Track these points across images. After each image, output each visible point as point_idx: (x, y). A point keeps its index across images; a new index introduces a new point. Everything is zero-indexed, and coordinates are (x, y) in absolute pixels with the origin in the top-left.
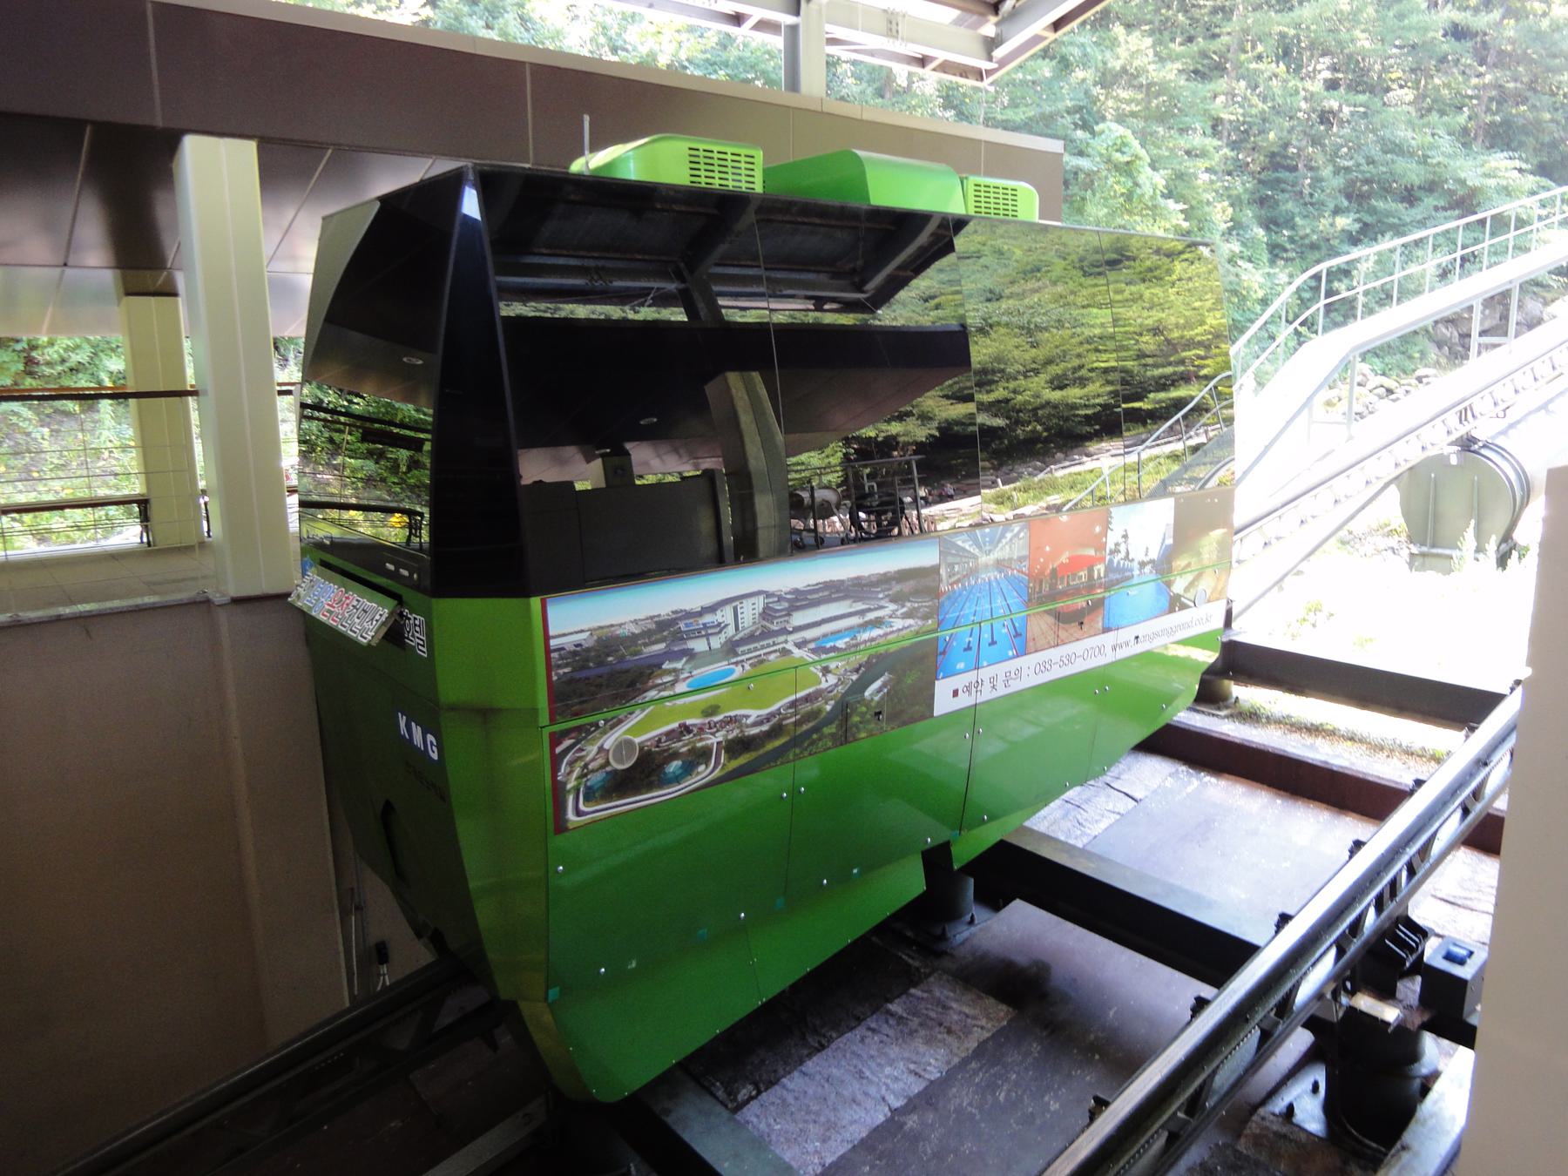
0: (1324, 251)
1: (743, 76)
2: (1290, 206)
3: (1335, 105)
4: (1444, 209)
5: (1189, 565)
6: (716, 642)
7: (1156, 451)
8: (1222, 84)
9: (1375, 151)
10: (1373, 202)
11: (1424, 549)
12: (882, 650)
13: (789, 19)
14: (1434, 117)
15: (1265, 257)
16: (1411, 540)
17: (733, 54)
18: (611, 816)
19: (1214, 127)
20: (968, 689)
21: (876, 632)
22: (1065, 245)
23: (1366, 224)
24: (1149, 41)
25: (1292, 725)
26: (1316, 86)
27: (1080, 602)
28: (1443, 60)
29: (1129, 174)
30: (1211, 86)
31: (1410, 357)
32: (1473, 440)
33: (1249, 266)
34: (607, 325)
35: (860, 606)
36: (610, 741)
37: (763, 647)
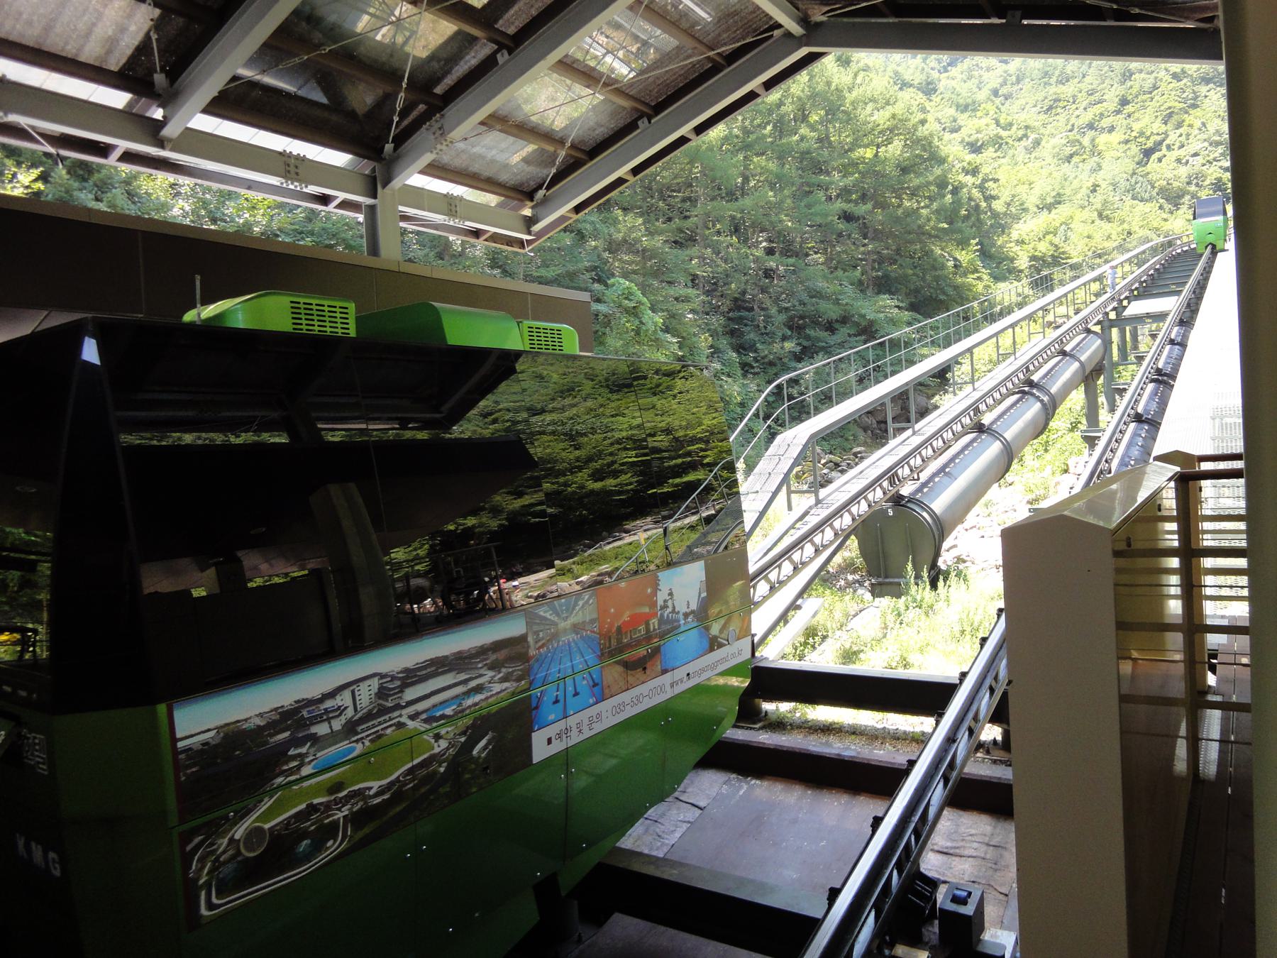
0: (779, 367)
1: (327, 242)
2: (752, 336)
3: (773, 265)
4: (855, 335)
5: (720, 611)
6: (337, 725)
7: (679, 524)
8: (695, 251)
9: (805, 297)
10: (808, 331)
12: (484, 712)
13: (369, 201)
14: (840, 273)
15: (739, 372)
16: (870, 574)
17: (317, 226)
18: (251, 901)
19: (693, 281)
20: (559, 736)
21: (478, 698)
22: (593, 369)
23: (805, 347)
24: (640, 220)
25: (810, 728)
26: (759, 253)
27: (642, 652)
28: (840, 235)
29: (636, 315)
30: (688, 252)
31: (847, 440)
32: (902, 497)
33: (730, 380)
34: (210, 450)
35: (463, 677)
36: (239, 832)
37: (380, 724)
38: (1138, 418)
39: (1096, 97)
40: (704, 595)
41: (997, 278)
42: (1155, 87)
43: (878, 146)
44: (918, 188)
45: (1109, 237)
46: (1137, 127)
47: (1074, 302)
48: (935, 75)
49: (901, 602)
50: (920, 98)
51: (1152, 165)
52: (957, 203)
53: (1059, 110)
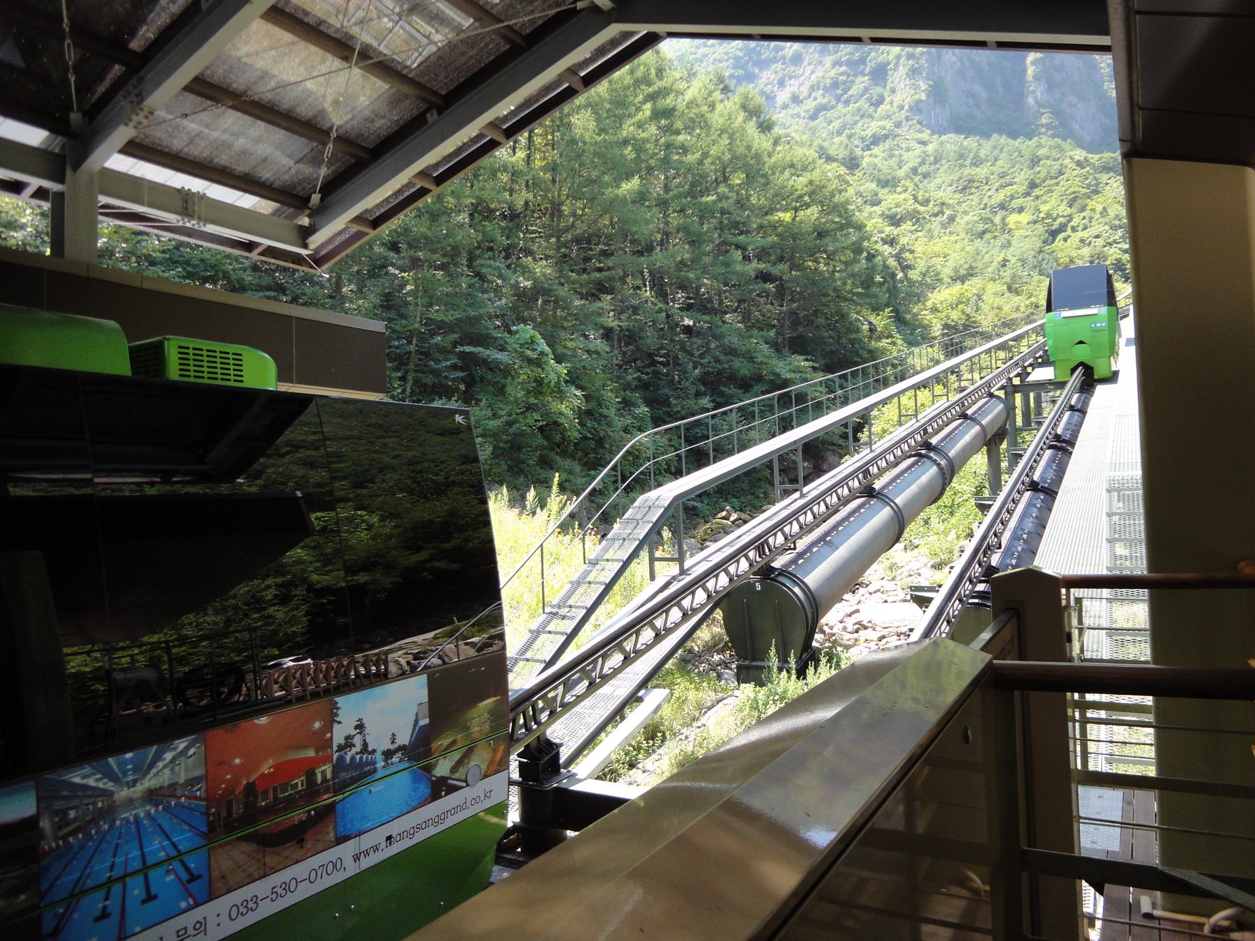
2: (666, 391)
5: (454, 743)
11: (747, 663)
27: (298, 815)
31: (758, 497)
38: (1034, 486)
41: (911, 344)
42: (1061, 173)
43: (796, 210)
44: (834, 252)
45: (1018, 309)
46: (1044, 208)
47: (983, 366)
48: (858, 152)
49: (763, 692)
50: (842, 170)
51: (1058, 243)
52: (872, 270)
53: (973, 190)
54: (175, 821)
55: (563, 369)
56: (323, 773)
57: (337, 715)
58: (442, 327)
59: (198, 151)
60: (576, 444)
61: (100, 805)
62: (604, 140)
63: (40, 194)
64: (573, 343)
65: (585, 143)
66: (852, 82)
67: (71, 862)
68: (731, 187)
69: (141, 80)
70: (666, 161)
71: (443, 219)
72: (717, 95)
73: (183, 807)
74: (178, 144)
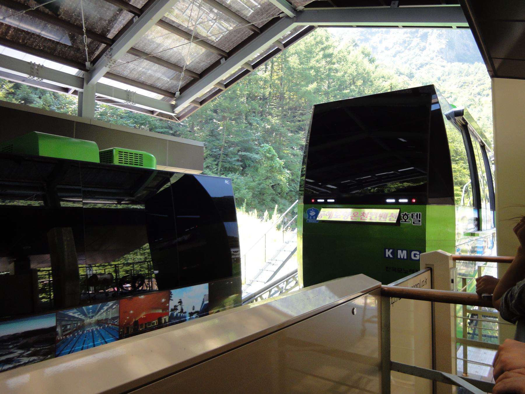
39: (482, 82)
40: (207, 302)
48: (414, 71)
50: (407, 78)
53: (466, 87)
54: (107, 333)
55: (282, 162)
56: (165, 319)
57: (171, 297)
58: (233, 144)
59: (132, 76)
60: (287, 193)
61: (79, 324)
62: (303, 68)
63: (75, 92)
64: (287, 151)
65: (294, 69)
66: (412, 41)
67: (67, 345)
68: (356, 86)
69: (112, 49)
70: (328, 76)
71: (235, 100)
72: (351, 48)
73: (110, 328)
74: (126, 73)
